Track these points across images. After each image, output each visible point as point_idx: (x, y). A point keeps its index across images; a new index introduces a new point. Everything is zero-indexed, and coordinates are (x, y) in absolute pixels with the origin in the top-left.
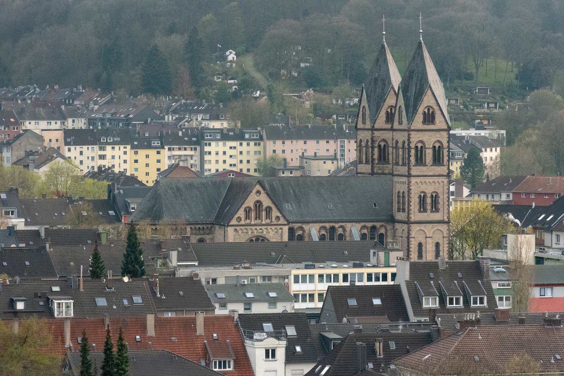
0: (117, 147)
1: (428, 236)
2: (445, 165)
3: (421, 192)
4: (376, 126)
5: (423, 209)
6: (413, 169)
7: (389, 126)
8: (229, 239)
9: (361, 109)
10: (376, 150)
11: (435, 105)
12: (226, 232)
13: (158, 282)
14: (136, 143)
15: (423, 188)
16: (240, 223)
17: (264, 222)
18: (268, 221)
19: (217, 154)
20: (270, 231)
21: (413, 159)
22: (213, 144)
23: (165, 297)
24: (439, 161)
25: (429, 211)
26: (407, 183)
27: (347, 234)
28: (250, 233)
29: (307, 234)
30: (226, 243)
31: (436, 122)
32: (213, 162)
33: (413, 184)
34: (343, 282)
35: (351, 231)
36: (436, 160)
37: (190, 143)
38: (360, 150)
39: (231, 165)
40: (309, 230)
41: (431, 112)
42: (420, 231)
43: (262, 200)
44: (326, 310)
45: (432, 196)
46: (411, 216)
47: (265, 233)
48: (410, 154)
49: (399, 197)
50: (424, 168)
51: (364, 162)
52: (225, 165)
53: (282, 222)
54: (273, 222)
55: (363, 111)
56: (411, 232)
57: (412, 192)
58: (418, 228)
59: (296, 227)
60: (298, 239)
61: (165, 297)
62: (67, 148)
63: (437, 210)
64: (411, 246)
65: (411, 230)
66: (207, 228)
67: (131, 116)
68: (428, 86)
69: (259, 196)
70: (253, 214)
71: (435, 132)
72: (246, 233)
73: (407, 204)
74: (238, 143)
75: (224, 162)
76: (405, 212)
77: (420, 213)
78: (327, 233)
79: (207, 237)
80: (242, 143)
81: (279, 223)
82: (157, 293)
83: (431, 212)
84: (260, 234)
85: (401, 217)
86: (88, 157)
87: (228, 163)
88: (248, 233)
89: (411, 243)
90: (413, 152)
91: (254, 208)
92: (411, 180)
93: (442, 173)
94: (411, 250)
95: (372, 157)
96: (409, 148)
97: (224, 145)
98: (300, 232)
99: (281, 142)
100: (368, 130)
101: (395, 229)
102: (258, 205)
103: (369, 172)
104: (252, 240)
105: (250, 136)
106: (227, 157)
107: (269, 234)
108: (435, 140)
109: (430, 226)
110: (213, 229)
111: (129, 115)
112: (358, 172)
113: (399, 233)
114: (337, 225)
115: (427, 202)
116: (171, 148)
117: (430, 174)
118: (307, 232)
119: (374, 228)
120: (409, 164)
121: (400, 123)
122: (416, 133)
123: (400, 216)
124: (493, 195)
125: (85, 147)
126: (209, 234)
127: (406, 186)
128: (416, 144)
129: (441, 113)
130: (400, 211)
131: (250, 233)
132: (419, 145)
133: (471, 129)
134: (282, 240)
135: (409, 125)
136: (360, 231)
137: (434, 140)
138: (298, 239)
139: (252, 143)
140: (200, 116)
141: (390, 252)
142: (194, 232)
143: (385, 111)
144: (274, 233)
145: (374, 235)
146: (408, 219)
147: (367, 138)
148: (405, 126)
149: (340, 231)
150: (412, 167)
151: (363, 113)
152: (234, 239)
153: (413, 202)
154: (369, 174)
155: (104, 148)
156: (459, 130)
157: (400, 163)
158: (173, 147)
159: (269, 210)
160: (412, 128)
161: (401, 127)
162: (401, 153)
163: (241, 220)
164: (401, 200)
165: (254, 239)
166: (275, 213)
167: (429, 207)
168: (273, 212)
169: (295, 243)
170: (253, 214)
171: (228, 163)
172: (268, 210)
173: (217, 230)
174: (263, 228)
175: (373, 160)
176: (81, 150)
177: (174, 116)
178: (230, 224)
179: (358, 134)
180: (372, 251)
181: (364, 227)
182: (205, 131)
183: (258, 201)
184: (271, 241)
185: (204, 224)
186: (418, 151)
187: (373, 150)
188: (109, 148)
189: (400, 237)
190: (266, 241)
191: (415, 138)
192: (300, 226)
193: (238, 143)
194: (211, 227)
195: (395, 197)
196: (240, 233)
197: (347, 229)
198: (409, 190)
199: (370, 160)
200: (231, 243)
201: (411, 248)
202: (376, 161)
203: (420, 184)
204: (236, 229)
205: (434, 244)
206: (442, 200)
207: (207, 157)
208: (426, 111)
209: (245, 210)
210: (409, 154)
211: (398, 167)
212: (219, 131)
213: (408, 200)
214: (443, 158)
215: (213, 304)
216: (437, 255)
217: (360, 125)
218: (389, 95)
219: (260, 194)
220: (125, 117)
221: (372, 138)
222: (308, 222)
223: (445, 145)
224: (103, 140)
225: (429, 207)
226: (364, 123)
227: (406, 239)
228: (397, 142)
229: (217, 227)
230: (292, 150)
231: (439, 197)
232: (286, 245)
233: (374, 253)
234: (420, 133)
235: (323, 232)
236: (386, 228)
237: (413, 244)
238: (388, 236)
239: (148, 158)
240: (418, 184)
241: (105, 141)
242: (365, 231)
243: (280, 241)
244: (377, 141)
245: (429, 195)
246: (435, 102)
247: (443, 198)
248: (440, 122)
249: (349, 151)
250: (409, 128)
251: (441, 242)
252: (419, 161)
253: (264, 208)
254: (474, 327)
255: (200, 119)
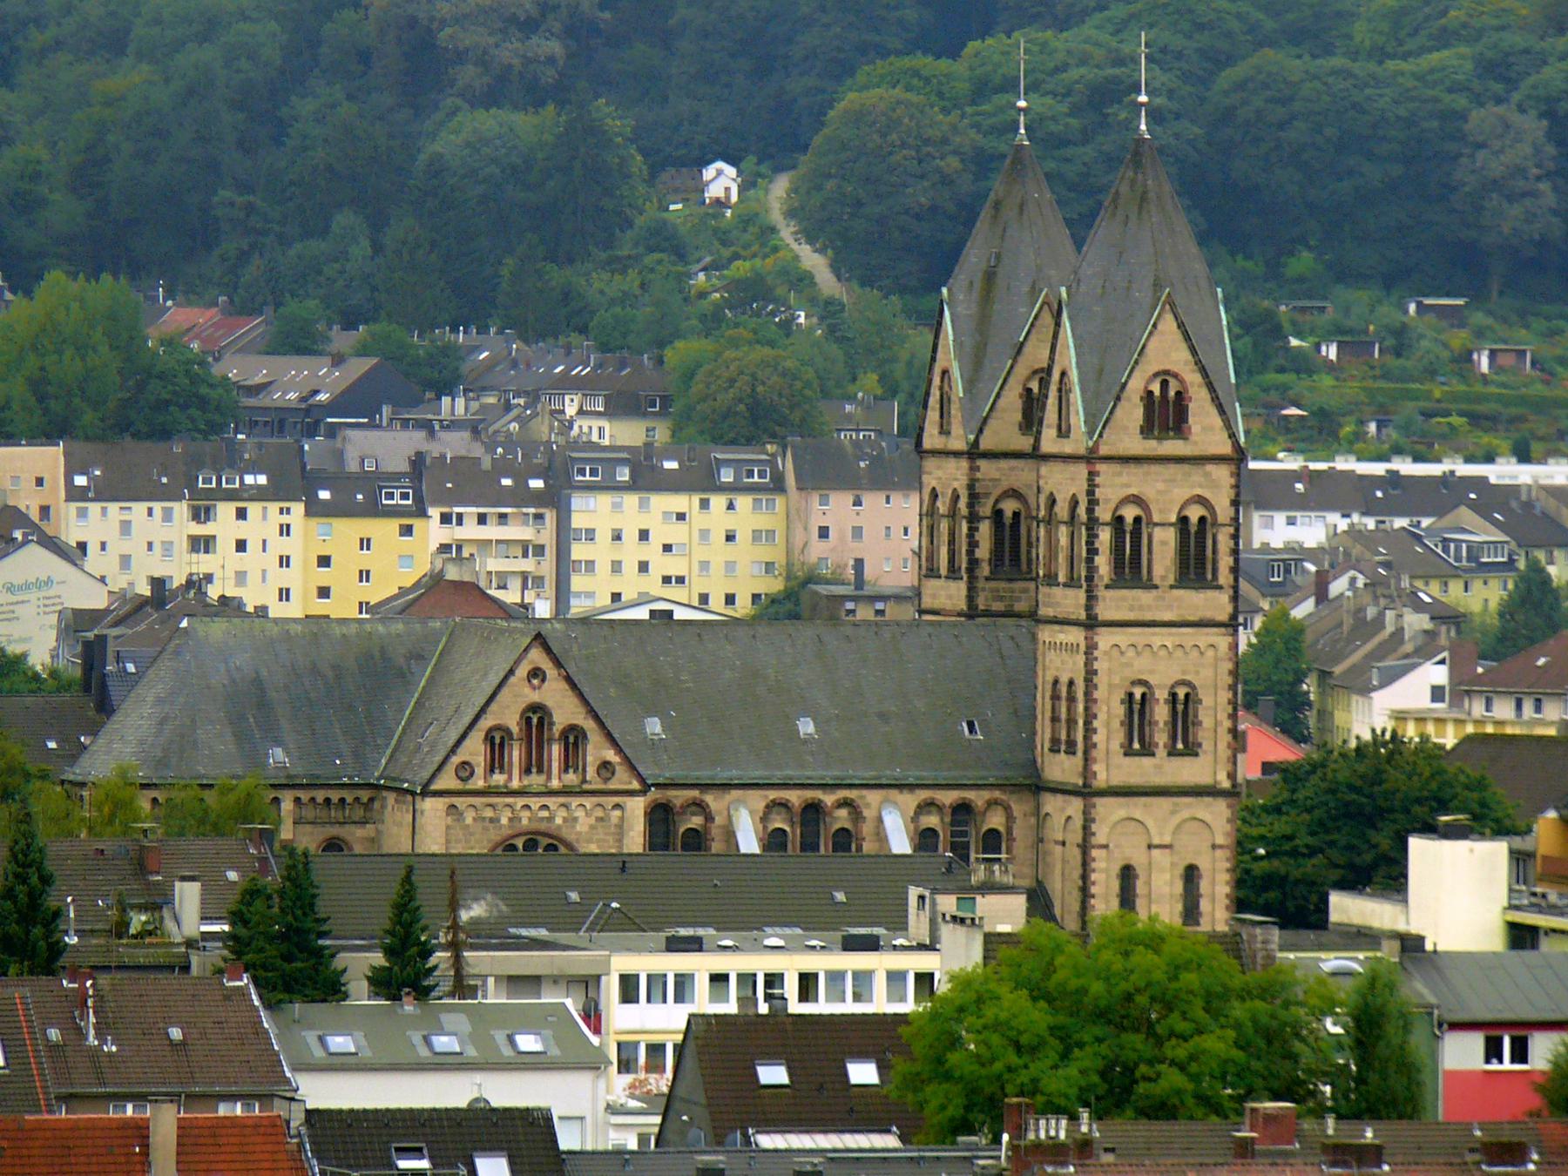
0: (254, 509)
1: (1156, 841)
2: (1156, 587)
3: (1133, 683)
4: (986, 443)
5: (1183, 743)
6: (1104, 599)
7: (1024, 443)
8: (428, 840)
9: (937, 381)
10: (985, 529)
11: (1187, 368)
12: (418, 815)
13: (91, 992)
14: (324, 495)
15: (1141, 666)
16: (470, 786)
17: (555, 784)
18: (571, 778)
19: (617, 537)
20: (580, 813)
21: (1103, 563)
22: (604, 501)
23: (114, 1049)
24: (1201, 575)
25: (1161, 752)
26: (1083, 648)
27: (867, 829)
28: (504, 821)
29: (719, 827)
30: (419, 855)
31: (1190, 428)
32: (603, 567)
33: (1106, 653)
34: (800, 1000)
35: (880, 820)
36: (1188, 568)
37: (521, 497)
38: (931, 529)
39: (667, 580)
40: (726, 813)
41: (1172, 393)
42: (1127, 823)
43: (549, 703)
44: (683, 1100)
45: (1174, 696)
46: (1096, 768)
47: (559, 821)
48: (1093, 543)
49: (1055, 697)
50: (1145, 597)
51: (943, 571)
52: (644, 577)
53: (621, 783)
54: (590, 783)
55: (941, 388)
56: (1094, 827)
57: (1101, 680)
58: (1122, 813)
59: (678, 803)
60: (685, 847)
61: (114, 1049)
62: (73, 506)
63: (1191, 750)
64: (1093, 877)
65: (1093, 820)
66: (357, 799)
67: (323, 397)
68: (1163, 298)
69: (539, 688)
70: (516, 754)
71: (1186, 467)
72: (492, 820)
73: (1081, 722)
74: (696, 499)
75: (643, 567)
76: (1074, 753)
77: (1127, 758)
78: (792, 824)
79: (357, 836)
80: (708, 501)
81: (612, 785)
82: (87, 1033)
83: (1170, 754)
84: (543, 827)
85: (1063, 771)
86: (150, 546)
87: (656, 572)
88: (498, 820)
89: (1094, 865)
90: (1105, 536)
91: (521, 730)
92: (1096, 638)
93: (1209, 614)
94: (1094, 890)
95: (970, 552)
96: (1092, 523)
97: (643, 505)
98: (696, 821)
99: (849, 498)
100: (956, 454)
101: (1043, 813)
102: (535, 721)
103: (958, 609)
104: (513, 848)
105: (737, 476)
106: (652, 552)
107: (574, 827)
108: (1187, 493)
109: (1164, 803)
110: (377, 805)
111: (316, 392)
112: (923, 606)
113: (1055, 830)
114: (829, 799)
115: (1157, 718)
116: (451, 514)
117: (1168, 616)
118: (719, 820)
119: (963, 810)
120: (1090, 579)
121: (1063, 432)
122: (1116, 467)
123: (1062, 768)
124: (1538, 701)
125: (140, 508)
126: (363, 822)
127: (1081, 659)
128: (1116, 509)
129: (1209, 397)
130: (1059, 751)
131: (504, 821)
132: (1130, 513)
133: (1551, 461)
134: (621, 847)
135: (1091, 438)
136: (915, 819)
137: (1182, 493)
138: (685, 847)
139: (744, 502)
140: (572, 400)
141: (979, 898)
142: (309, 813)
143: (1020, 389)
144: (592, 821)
145: (965, 834)
146: (1085, 778)
147: (956, 484)
148: (1078, 442)
149: (842, 817)
150: (1101, 592)
151: (942, 396)
152: (448, 841)
153: (1102, 716)
154: (959, 615)
155: (207, 510)
156: (1508, 463)
157: (1062, 578)
158: (457, 510)
159: (573, 739)
160: (1104, 450)
161: (1067, 447)
162: (1063, 540)
163: (472, 774)
164: (1064, 710)
165: (520, 843)
166: (597, 751)
167: (1161, 738)
168: (589, 747)
169: (677, 859)
170: (516, 754)
171: (656, 572)
172: (571, 739)
173: (390, 808)
174: (551, 802)
175: (973, 563)
176: (127, 518)
177: (473, 399)
178: (434, 787)
179: (927, 469)
180: (913, 893)
181: (926, 807)
182: (574, 455)
183: (536, 708)
184: (582, 850)
185: (344, 785)
186: (1124, 532)
187: (972, 530)
188: (226, 510)
189: (1057, 842)
190: (563, 850)
191: (1114, 485)
192: (695, 798)
193: (696, 499)
194: (372, 800)
195: (1043, 698)
196: (469, 821)
197: (866, 813)
198: (1090, 673)
199: (964, 566)
200: (434, 855)
201: (1094, 883)
202: (985, 570)
203: (1131, 653)
204: (453, 806)
205: (1180, 870)
206: (1211, 712)
207: (578, 552)
208: (1156, 388)
209: (489, 738)
210: (1090, 543)
211: (1055, 590)
212: (625, 455)
213: (1086, 709)
214: (1215, 562)
215: (288, 1074)
216: (1191, 912)
217: (931, 439)
218: (1034, 331)
219: (543, 680)
220: (303, 399)
221: (971, 487)
222: (726, 786)
223: (1224, 511)
224: (207, 481)
225: (1161, 738)
226: (944, 431)
227: (1077, 852)
228: (1052, 501)
229: (391, 797)
230: (888, 528)
231: (1200, 701)
232: (624, 863)
233: (922, 898)
234: (1133, 468)
235: (778, 823)
236: (1008, 809)
237: (1102, 871)
238: (1014, 840)
239: (368, 549)
240: (1122, 653)
241: (214, 485)
242: (932, 821)
243: (613, 851)
244: (987, 495)
245: (1162, 695)
246: (1190, 357)
247: (1212, 704)
248: (1207, 429)
249: (906, 534)
250: (1093, 450)
251: (1204, 864)
252: (1127, 570)
253: (557, 729)
254: (1064, 1164)
255: (571, 410)
